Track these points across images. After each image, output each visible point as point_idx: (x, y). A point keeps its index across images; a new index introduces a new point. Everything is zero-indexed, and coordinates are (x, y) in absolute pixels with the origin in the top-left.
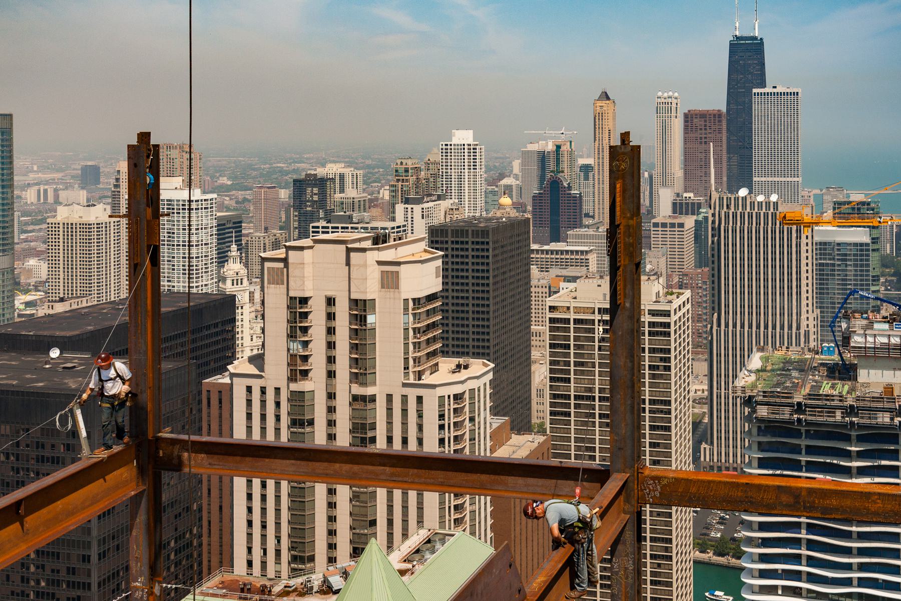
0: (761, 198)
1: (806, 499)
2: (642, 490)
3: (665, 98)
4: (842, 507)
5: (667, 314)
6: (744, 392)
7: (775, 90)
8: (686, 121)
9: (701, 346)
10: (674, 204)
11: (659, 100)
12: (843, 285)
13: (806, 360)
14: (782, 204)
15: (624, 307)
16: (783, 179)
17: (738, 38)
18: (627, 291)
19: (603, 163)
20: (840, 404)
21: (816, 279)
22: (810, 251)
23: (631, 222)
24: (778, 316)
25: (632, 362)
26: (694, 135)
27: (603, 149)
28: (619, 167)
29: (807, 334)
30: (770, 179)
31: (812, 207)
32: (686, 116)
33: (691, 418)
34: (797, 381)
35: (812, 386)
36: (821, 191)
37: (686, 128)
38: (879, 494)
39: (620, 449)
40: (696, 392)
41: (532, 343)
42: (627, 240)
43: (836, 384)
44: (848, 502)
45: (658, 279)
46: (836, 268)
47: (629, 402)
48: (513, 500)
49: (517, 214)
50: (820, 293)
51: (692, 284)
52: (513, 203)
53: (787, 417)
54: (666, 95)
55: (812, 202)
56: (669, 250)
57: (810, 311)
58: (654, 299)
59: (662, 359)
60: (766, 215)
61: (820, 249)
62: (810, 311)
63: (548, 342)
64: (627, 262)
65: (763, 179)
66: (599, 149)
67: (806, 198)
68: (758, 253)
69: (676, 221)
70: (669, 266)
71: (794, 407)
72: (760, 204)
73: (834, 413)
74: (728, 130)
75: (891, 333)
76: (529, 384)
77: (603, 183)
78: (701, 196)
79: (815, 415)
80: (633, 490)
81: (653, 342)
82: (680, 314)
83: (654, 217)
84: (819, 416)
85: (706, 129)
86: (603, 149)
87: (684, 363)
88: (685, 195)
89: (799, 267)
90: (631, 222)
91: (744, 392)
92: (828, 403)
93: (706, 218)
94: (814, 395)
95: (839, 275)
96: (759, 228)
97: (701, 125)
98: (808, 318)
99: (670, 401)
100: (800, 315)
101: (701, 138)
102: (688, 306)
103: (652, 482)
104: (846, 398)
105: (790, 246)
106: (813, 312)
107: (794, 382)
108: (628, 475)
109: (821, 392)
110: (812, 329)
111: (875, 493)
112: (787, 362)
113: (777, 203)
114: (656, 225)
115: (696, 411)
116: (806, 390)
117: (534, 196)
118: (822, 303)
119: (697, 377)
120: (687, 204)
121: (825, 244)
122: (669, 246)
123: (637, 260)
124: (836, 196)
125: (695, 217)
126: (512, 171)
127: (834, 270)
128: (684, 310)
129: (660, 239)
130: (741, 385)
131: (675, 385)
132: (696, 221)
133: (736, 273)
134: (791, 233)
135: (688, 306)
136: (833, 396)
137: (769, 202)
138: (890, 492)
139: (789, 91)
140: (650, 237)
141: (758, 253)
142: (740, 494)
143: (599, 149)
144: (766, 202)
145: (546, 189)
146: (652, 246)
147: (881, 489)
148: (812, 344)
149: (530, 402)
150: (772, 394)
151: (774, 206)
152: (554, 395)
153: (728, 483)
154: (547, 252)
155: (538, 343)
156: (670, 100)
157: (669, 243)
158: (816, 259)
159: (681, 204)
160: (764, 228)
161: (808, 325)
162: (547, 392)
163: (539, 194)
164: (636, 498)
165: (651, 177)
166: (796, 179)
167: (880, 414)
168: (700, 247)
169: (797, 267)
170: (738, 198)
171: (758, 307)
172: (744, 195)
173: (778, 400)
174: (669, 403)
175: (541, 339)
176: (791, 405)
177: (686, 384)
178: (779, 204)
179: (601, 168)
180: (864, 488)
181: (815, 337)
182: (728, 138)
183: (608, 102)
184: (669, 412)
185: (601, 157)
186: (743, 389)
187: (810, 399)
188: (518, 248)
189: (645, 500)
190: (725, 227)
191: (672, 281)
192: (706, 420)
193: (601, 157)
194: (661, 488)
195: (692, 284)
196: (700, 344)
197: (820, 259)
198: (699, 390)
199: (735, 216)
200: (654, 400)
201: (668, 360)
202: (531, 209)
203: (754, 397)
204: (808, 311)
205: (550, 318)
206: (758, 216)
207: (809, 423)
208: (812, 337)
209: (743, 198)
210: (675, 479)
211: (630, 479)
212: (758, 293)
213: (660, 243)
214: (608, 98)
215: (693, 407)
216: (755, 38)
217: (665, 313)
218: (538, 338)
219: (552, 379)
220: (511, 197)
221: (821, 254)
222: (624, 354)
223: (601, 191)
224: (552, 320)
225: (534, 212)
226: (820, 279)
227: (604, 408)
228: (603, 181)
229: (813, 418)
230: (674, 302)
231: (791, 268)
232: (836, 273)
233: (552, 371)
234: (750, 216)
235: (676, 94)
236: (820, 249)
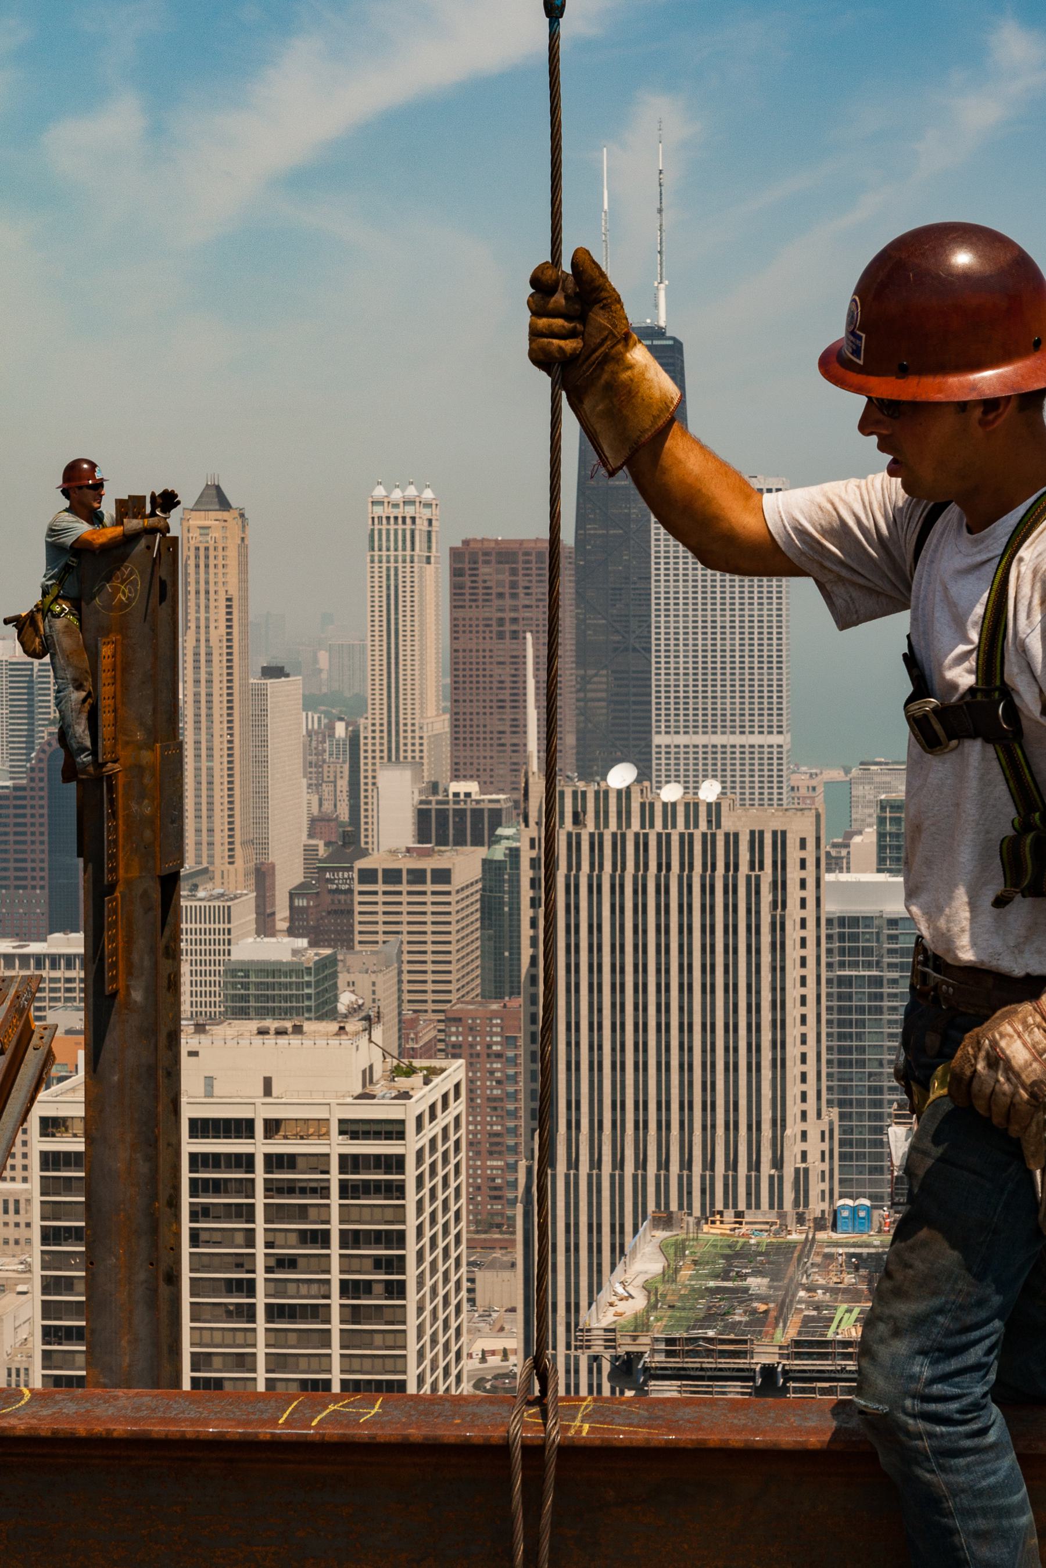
5: (394, 1130)
16: (738, 739)
59: (379, 1263)
69: (428, 864)
72: (670, 809)
88: (455, 787)
114: (368, 876)
120: (460, 813)
127: (880, 997)
128: (445, 1119)
135: (458, 1107)
212: (665, 1067)
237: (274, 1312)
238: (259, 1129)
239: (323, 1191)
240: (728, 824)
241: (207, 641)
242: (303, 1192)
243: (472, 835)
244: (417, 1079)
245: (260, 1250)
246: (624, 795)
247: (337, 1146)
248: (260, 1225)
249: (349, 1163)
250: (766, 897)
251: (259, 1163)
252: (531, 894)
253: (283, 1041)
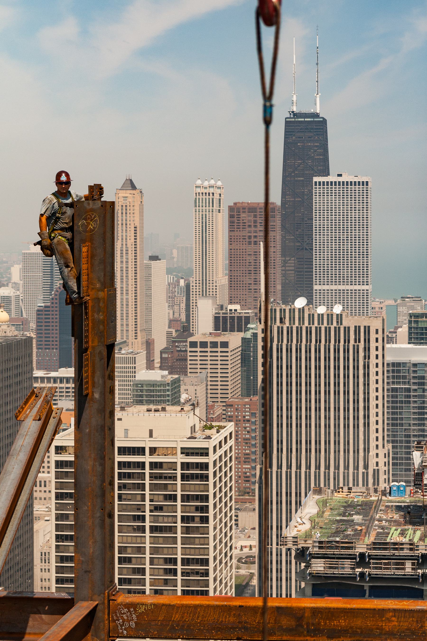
0: (321, 310)
1: (310, 621)
2: (114, 621)
3: (206, 188)
4: (351, 628)
5: (204, 452)
6: (295, 543)
7: (340, 179)
8: (231, 216)
9: (248, 493)
10: (216, 319)
11: (198, 190)
12: (420, 413)
13: (372, 502)
14: (347, 316)
15: (93, 399)
16: (349, 287)
17: (295, 115)
18: (96, 380)
19: (127, 268)
20: (411, 553)
21: (388, 407)
22: (380, 373)
23: (101, 294)
24: (342, 453)
25: (103, 465)
26: (242, 234)
27: (127, 250)
28: (87, 227)
29: (376, 473)
30: (334, 287)
31: (383, 320)
32: (231, 209)
33: (233, 580)
34: (360, 528)
35: (378, 534)
36: (396, 301)
37: (231, 224)
38: (395, 610)
39: (86, 572)
40: (241, 550)
42: (96, 316)
43: (406, 530)
44: (358, 622)
45: (194, 409)
46: (412, 394)
47: (98, 515)
49: (16, 333)
50: (393, 425)
51: (237, 417)
52: (11, 320)
53: (348, 571)
54: (206, 184)
55: (384, 314)
56: (209, 375)
57: (380, 446)
58: (189, 435)
59: (197, 509)
60: (328, 331)
61: (393, 371)
62: (380, 446)
63: (54, 491)
64: (96, 343)
65: (326, 287)
66: (122, 250)
67: (377, 309)
68: (318, 376)
70: (209, 396)
71: (355, 559)
73: (403, 564)
74: (283, 227)
76: (31, 546)
77: (127, 294)
78: (250, 309)
79: (380, 568)
80: (104, 621)
81: (187, 488)
82: (220, 452)
83: (192, 335)
84: (385, 569)
85: (255, 226)
86: (127, 250)
87: (226, 513)
88: (230, 307)
89: (367, 393)
90: (101, 294)
91: (295, 543)
92: (396, 553)
93: (255, 335)
94: (380, 544)
95: (415, 402)
96: (320, 346)
97: (249, 221)
98: (377, 455)
99: (207, 560)
100: (369, 452)
101: (250, 237)
102: (231, 442)
103: (126, 610)
104: (417, 546)
105: (356, 368)
106: (384, 447)
107: (356, 530)
108: (96, 603)
109: (388, 540)
110: (382, 468)
111: (389, 609)
112: (349, 506)
113: (341, 315)
114: (193, 344)
115: (243, 572)
116: (371, 539)
117: (38, 311)
118: (394, 436)
119: (243, 530)
120: (232, 318)
121: (399, 364)
122: (209, 371)
123: (109, 342)
124: (412, 308)
125: (241, 335)
126: (10, 279)
127: (409, 397)
128: (226, 447)
129: (199, 362)
130: (293, 535)
131: (215, 540)
132: (243, 339)
133: (291, 402)
134: (358, 352)
135: (231, 442)
136: (402, 544)
137: (332, 315)
138: (406, 607)
139: (357, 180)
140: (186, 360)
141: (318, 376)
142: (232, 619)
143: (122, 250)
144: (328, 315)
145: (55, 301)
146: (189, 371)
147: (397, 605)
148: (382, 486)
149: (31, 569)
150: (329, 545)
151: (337, 319)
152: (62, 557)
153: (218, 606)
154: (55, 380)
156: (211, 190)
157: (209, 366)
158: (388, 383)
159: (225, 318)
160: (325, 346)
161: (377, 463)
162: (53, 554)
163: (46, 307)
164: (106, 631)
165: (188, 286)
166: (365, 287)
168: (248, 371)
169: (364, 393)
170: (294, 310)
171: (318, 442)
172: (301, 306)
173: (337, 552)
174: (206, 562)
175: (47, 489)
176: (351, 557)
177: (228, 538)
178: (344, 317)
179: (125, 275)
180: (377, 605)
181: (386, 477)
182: (283, 238)
183: (134, 192)
184: (207, 574)
185: (124, 260)
186: (295, 540)
187: (375, 549)
188: (16, 375)
189: (118, 633)
190: (278, 345)
191: (213, 414)
192: (255, 582)
193: (124, 260)
194: (137, 617)
195: (237, 417)
196: (248, 490)
197: (393, 383)
198: (246, 547)
199: (290, 331)
200: (188, 559)
201: (206, 509)
202: (35, 326)
203: (308, 548)
204: (377, 446)
205: (57, 462)
206: (318, 331)
207: (373, 578)
208: (382, 477)
209: (299, 309)
210: (154, 605)
211: (99, 607)
213: (199, 366)
214: (134, 187)
215: (238, 568)
216: (317, 115)
217: (202, 451)
218: (43, 489)
219: (58, 538)
220: (9, 311)
221: (393, 377)
222: (93, 456)
223: (125, 303)
225: (38, 330)
226: (393, 408)
227: (125, 571)
228: (127, 290)
229: (378, 572)
230: (214, 437)
231: (358, 394)
232: (412, 399)
233: (58, 527)
234: (309, 332)
235: (219, 183)
236: (393, 371)
237: (153, 529)
238: (147, 451)
240: (345, 323)
241: (126, 245)
245: (147, 503)
246: (302, 311)
247: (180, 459)
248: (147, 492)
250: (361, 354)
251: (147, 466)
253: (157, 414)
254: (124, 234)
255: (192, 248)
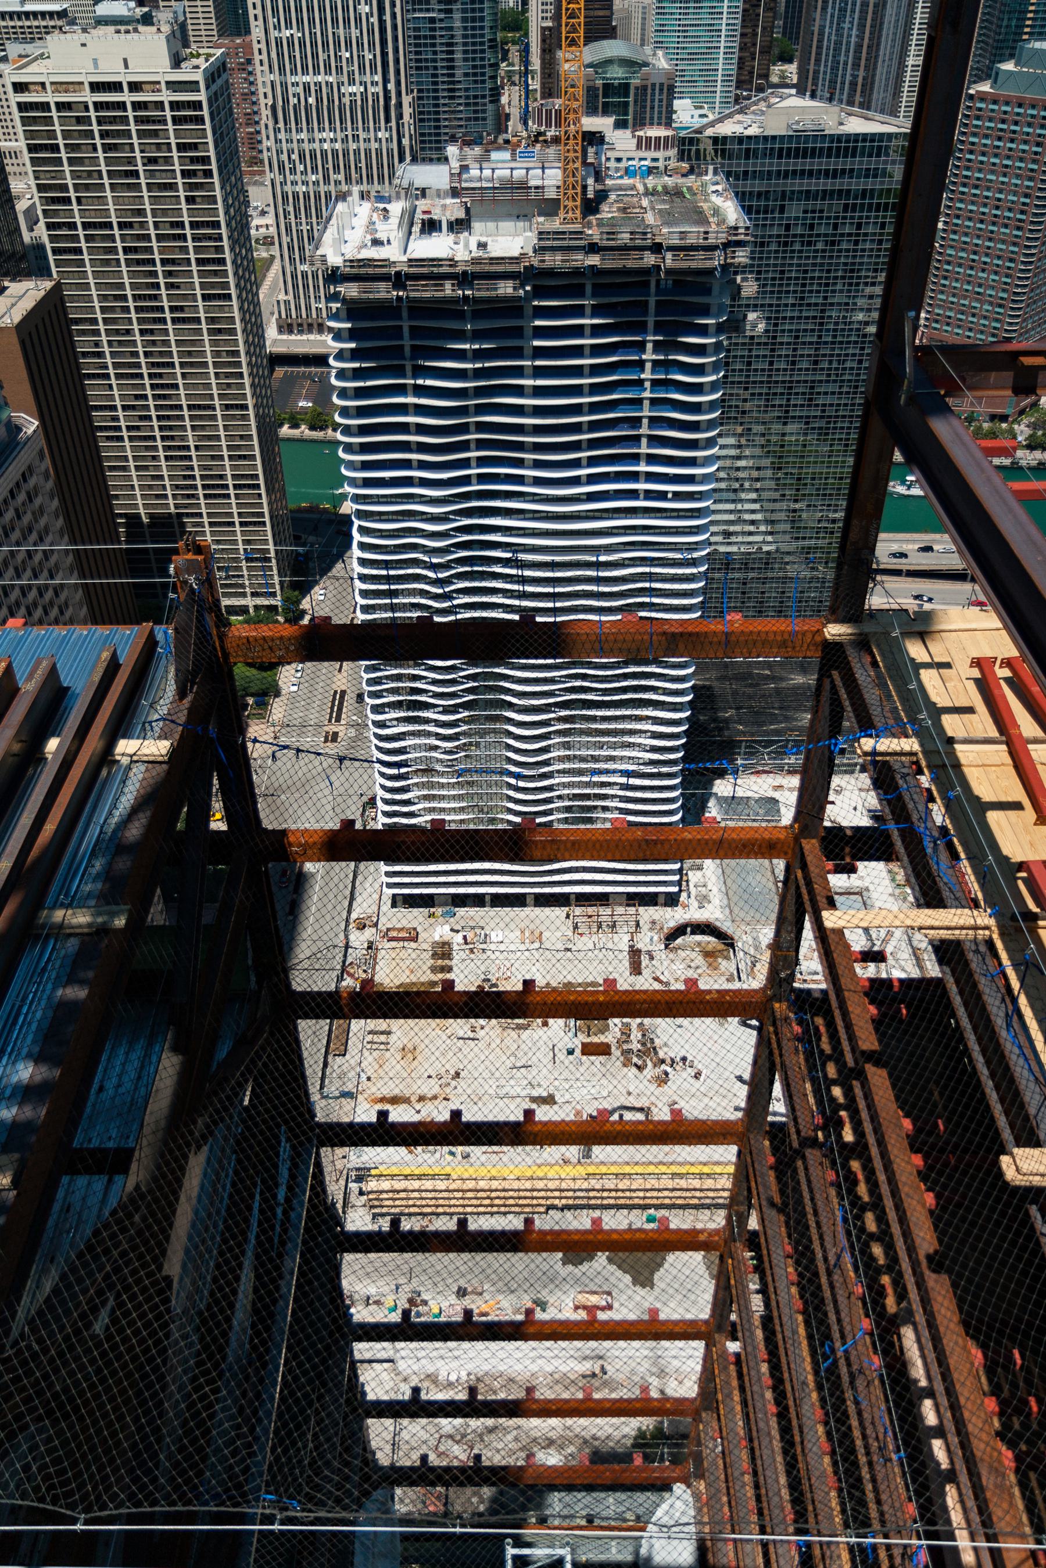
41: (8, 169)
48: (731, 1547)
75: (513, 165)
92: (435, 270)
127: (434, 29)
155: (16, 169)
167: (501, 284)
224: (22, 107)
239: (164, 122)
242: (154, 122)
243: (1015, 966)
244: (202, 59)
249: (175, 105)
251: (129, 107)
252: (643, 463)
253: (129, 36)
254: (469, 1195)
255: (405, 1537)
